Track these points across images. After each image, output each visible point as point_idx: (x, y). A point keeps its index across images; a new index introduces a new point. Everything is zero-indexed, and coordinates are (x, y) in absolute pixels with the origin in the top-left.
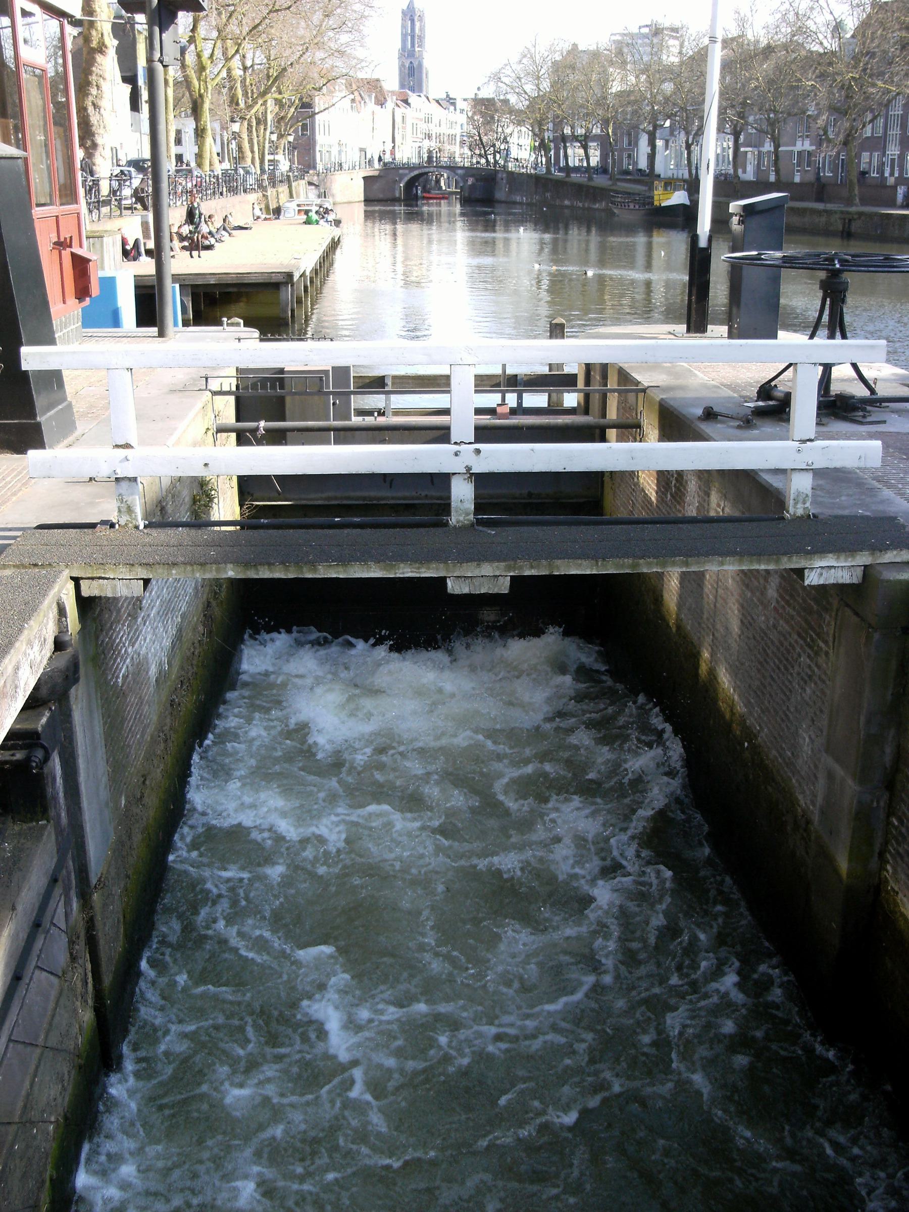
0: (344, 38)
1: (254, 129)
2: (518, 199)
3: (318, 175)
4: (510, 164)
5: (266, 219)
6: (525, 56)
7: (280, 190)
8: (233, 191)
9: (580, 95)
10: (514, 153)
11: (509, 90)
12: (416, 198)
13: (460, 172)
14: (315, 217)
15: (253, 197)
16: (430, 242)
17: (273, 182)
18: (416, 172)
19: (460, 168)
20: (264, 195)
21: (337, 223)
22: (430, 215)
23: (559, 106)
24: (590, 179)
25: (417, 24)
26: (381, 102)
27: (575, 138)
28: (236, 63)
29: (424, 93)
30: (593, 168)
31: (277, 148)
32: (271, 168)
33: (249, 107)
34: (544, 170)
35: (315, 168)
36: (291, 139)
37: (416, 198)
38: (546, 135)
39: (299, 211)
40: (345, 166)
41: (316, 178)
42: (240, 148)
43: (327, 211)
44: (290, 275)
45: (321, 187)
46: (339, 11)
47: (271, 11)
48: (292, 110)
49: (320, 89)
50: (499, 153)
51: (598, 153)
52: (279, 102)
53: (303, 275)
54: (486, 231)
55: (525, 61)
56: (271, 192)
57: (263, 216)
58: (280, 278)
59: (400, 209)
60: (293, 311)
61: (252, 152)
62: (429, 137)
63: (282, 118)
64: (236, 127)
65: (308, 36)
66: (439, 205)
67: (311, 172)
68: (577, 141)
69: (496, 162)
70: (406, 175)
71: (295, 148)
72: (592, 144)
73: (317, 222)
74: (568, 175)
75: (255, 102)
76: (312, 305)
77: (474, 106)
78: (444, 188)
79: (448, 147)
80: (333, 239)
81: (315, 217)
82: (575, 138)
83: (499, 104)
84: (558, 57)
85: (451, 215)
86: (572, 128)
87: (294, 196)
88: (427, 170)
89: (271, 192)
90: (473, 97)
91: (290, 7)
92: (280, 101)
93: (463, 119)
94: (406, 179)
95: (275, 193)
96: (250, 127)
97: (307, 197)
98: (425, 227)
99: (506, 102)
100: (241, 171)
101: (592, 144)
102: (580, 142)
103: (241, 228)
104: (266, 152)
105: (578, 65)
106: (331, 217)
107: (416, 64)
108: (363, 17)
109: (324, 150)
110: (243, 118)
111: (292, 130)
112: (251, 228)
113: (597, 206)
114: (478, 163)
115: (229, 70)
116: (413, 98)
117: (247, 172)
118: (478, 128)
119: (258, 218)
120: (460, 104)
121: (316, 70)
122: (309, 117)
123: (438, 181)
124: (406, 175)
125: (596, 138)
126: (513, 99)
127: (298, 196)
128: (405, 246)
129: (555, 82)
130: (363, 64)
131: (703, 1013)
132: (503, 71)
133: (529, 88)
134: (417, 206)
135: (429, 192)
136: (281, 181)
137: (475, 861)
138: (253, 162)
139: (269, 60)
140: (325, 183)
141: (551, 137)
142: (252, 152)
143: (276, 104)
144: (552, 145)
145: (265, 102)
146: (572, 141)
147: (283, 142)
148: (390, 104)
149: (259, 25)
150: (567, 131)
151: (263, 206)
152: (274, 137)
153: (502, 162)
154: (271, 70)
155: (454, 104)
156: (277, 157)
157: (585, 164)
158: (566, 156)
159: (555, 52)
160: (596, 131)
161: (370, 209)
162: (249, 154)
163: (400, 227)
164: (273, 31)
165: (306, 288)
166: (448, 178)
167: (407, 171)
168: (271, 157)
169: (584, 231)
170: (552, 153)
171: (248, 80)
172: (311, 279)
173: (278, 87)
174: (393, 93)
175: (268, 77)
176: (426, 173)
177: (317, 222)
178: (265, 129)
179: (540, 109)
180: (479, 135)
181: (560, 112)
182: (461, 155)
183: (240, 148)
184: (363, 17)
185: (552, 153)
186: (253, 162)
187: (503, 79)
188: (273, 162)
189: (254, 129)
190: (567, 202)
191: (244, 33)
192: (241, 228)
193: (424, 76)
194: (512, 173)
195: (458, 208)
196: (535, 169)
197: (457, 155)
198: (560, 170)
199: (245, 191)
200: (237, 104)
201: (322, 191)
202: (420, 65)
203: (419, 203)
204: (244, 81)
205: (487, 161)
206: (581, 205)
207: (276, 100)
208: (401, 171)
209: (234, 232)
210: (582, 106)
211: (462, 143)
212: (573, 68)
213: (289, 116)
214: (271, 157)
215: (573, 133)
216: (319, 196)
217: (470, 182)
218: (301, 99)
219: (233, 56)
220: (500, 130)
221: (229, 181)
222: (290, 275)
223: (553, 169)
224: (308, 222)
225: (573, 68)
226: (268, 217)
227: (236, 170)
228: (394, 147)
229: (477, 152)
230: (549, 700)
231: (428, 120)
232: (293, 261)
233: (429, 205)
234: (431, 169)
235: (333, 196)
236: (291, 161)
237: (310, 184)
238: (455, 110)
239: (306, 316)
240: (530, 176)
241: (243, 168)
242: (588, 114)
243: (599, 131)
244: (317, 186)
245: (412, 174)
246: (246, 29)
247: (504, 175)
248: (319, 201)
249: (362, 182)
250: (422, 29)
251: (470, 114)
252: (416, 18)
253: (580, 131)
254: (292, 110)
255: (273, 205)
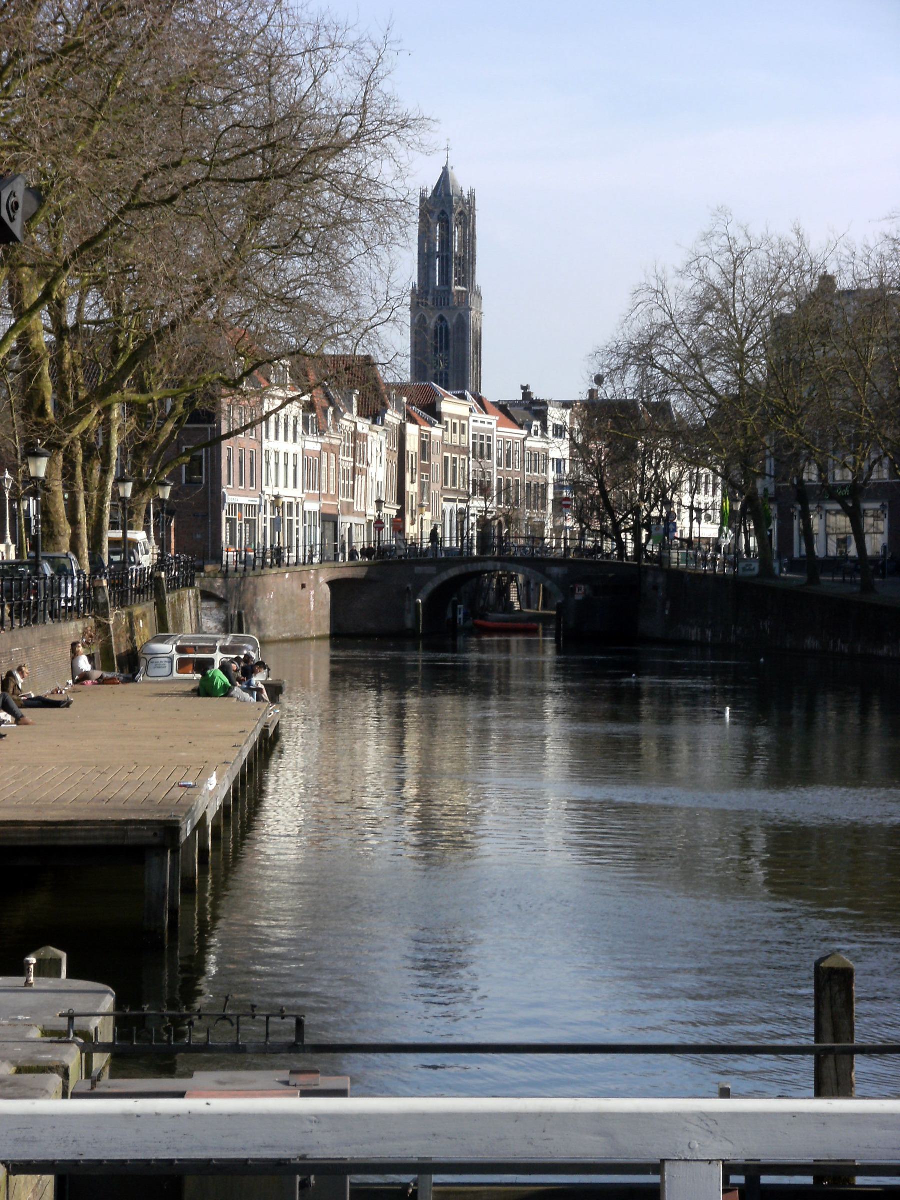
0: (296, 266)
1: (79, 470)
2: (694, 634)
3: (226, 575)
4: (674, 555)
5: (102, 681)
6: (710, 308)
7: (138, 611)
8: (28, 614)
9: (839, 392)
10: (683, 524)
11: (672, 384)
12: (453, 630)
13: (556, 571)
14: (221, 679)
15: (73, 629)
16: (483, 734)
17: (122, 596)
18: (453, 572)
19: (556, 562)
20: (99, 625)
21: (275, 691)
22: (484, 670)
23: (792, 419)
24: (868, 587)
25: (457, 233)
26: (374, 414)
27: (829, 492)
28: (43, 318)
29: (471, 386)
30: (874, 561)
31: (131, 514)
32: (117, 558)
33: (71, 421)
34: (756, 566)
35: (218, 558)
36: (166, 493)
37: (453, 630)
38: (760, 484)
39: (183, 664)
40: (291, 557)
41: (219, 582)
42: (45, 511)
43: (249, 668)
44: (171, 829)
45: (233, 602)
46: (282, 208)
47: (129, 207)
48: (170, 427)
49: (235, 384)
50: (648, 527)
51: (883, 525)
52: (132, 408)
53: (201, 825)
54: (615, 718)
55: (710, 318)
56: (115, 618)
57: (97, 674)
58: (148, 836)
59: (418, 657)
60: (174, 912)
61: (74, 521)
62: (484, 490)
63: (145, 445)
64: (40, 468)
65: (212, 264)
66: (506, 648)
67: (209, 568)
68: (833, 498)
69: (640, 548)
70: (430, 577)
71: (171, 513)
72: (870, 506)
73: (227, 692)
74: (813, 579)
75: (83, 408)
76: (217, 896)
77: (587, 424)
78: (517, 607)
79: (528, 513)
80: (264, 732)
81: (221, 679)
82: (829, 492)
83: (647, 416)
84: (785, 307)
85: (533, 670)
86: (822, 469)
87: (170, 624)
88: (479, 567)
89: (115, 618)
90: (585, 397)
91: (174, 197)
92: (142, 407)
93: (560, 449)
94: (430, 587)
95: (124, 620)
96: (69, 462)
97: (199, 629)
98: (472, 705)
99: (663, 409)
100: (48, 570)
101: (870, 506)
102: (841, 501)
103: (42, 703)
104: (107, 521)
105: (836, 326)
106: (258, 679)
107: (452, 322)
108: (340, 221)
109: (240, 519)
110: (53, 446)
111: (167, 472)
112: (67, 704)
113: (885, 651)
114: (598, 549)
115: (25, 338)
116: (450, 406)
117: (62, 571)
118: (597, 470)
119: (85, 677)
120: (555, 415)
121: (227, 338)
122: (206, 446)
123: (504, 591)
124: (430, 577)
125: (879, 491)
126: (679, 405)
127: (179, 627)
128: (426, 752)
129: (779, 365)
130: (338, 328)
131: (487, 480)
132: (660, 341)
133: (719, 378)
134: (454, 650)
135: (483, 617)
136: (139, 591)
137: (884, 820)
138: (75, 547)
139: (117, 311)
140: (241, 594)
141: (772, 490)
142: (74, 521)
143: (130, 415)
144: (774, 509)
145: (108, 410)
146: (821, 500)
147: (146, 499)
148: (393, 417)
149: (101, 236)
150: (811, 475)
151: (96, 650)
152: (127, 490)
153: (652, 548)
154: (122, 338)
155: (542, 416)
156: (131, 535)
157: (853, 551)
158: (808, 535)
159: (781, 296)
160: (881, 474)
161: (342, 654)
162: (66, 529)
163: (413, 701)
164: (130, 249)
165: (204, 852)
166: (527, 583)
167: (431, 570)
168: (118, 534)
169: (853, 718)
170: (774, 526)
171: (68, 358)
172: (216, 829)
173: (139, 377)
174: (402, 389)
175: (116, 352)
176: (479, 574)
177: (227, 692)
178: (105, 472)
179: (744, 426)
180: (601, 487)
181: (792, 434)
182: (558, 530)
183: (45, 511)
184: (340, 221)
185: (774, 526)
186: (75, 547)
187: (661, 360)
188: (126, 547)
189: (79, 470)
190: (811, 643)
191: (65, 254)
192: (42, 703)
193: (471, 348)
194: (678, 575)
195: (549, 655)
196: (734, 565)
197: (547, 532)
198: (794, 566)
199: (54, 615)
200: (42, 412)
201: (234, 612)
202: (463, 325)
203: (460, 641)
204: (58, 361)
205: (622, 547)
206: (845, 648)
207: (131, 404)
208: (418, 570)
209: (27, 713)
210: (846, 420)
211: (560, 505)
212: (824, 332)
213: (162, 440)
214: (118, 534)
215: (823, 480)
216: (227, 628)
217: (579, 596)
218: (190, 403)
219: (36, 306)
220: (650, 474)
221: (19, 590)
222: (171, 829)
223: (776, 565)
224: (206, 690)
225: (824, 332)
226: (107, 675)
227: (35, 565)
228: (401, 514)
229: (596, 526)
230: (765, 874)
231: (481, 451)
232: (179, 793)
233: (482, 648)
234: (490, 566)
235: (259, 624)
236: (163, 544)
237: (207, 596)
238: (545, 428)
239: (203, 924)
240: (720, 580)
241: (52, 561)
242: (857, 439)
243: (885, 474)
244: (222, 602)
245: (445, 576)
246: (67, 244)
247: (661, 580)
248: (228, 640)
249: (327, 589)
250: (469, 242)
251: (580, 440)
252: (454, 217)
253: (842, 476)
254: (170, 427)
255: (120, 647)
